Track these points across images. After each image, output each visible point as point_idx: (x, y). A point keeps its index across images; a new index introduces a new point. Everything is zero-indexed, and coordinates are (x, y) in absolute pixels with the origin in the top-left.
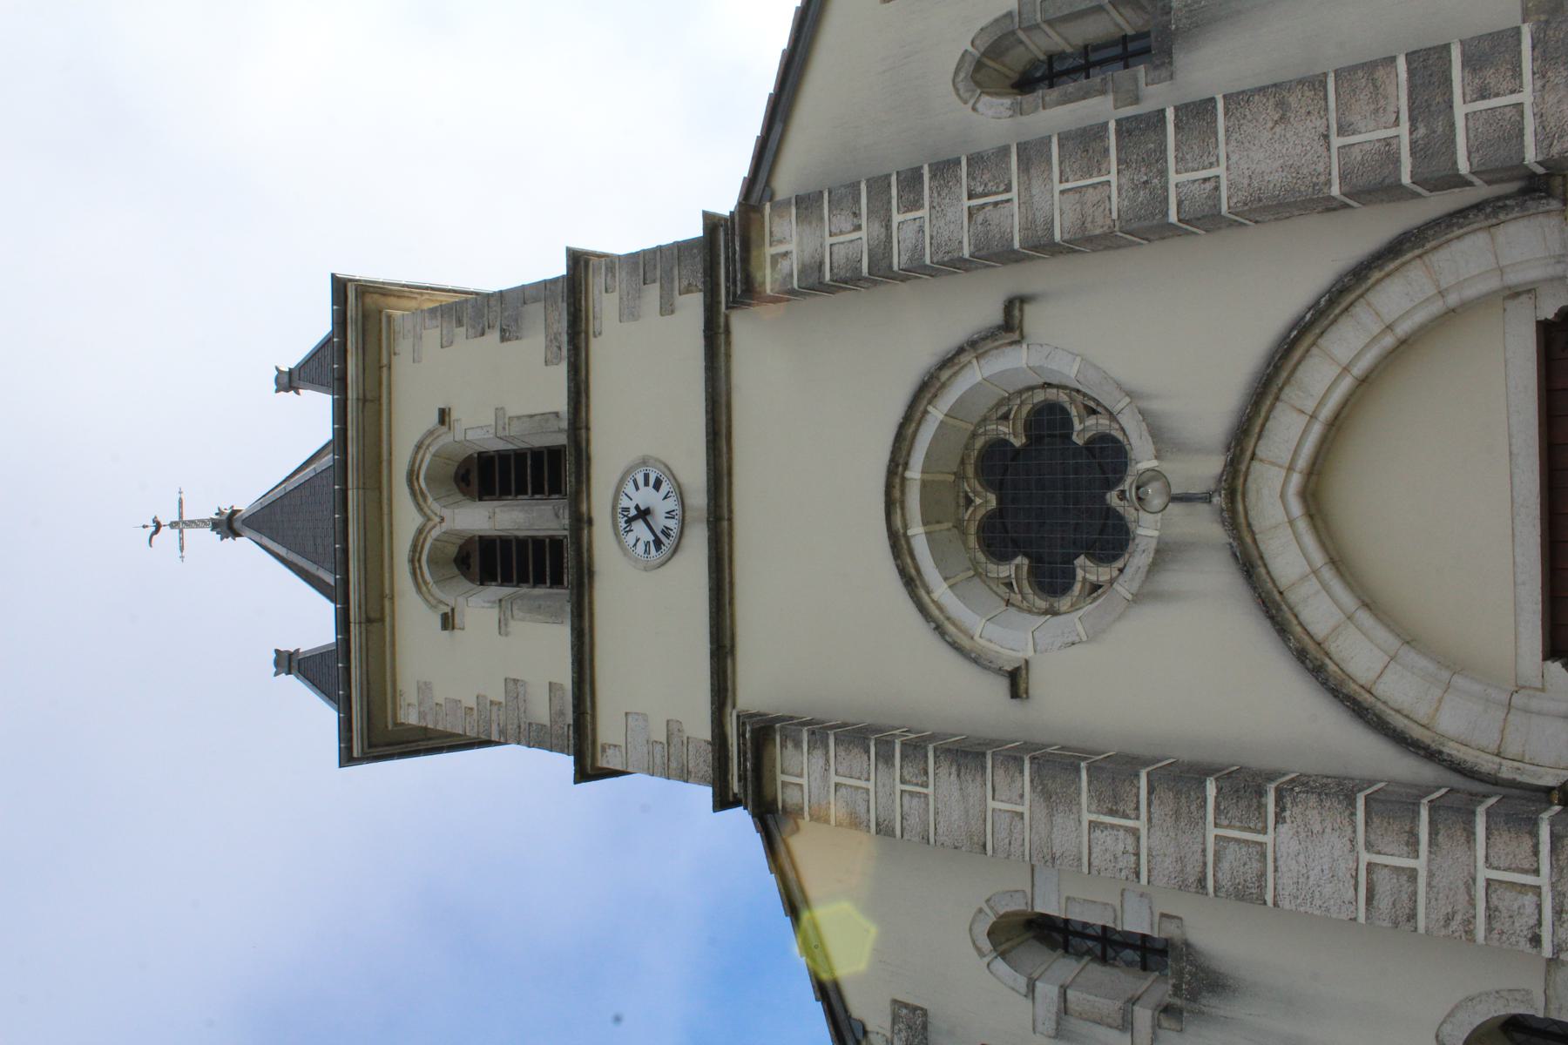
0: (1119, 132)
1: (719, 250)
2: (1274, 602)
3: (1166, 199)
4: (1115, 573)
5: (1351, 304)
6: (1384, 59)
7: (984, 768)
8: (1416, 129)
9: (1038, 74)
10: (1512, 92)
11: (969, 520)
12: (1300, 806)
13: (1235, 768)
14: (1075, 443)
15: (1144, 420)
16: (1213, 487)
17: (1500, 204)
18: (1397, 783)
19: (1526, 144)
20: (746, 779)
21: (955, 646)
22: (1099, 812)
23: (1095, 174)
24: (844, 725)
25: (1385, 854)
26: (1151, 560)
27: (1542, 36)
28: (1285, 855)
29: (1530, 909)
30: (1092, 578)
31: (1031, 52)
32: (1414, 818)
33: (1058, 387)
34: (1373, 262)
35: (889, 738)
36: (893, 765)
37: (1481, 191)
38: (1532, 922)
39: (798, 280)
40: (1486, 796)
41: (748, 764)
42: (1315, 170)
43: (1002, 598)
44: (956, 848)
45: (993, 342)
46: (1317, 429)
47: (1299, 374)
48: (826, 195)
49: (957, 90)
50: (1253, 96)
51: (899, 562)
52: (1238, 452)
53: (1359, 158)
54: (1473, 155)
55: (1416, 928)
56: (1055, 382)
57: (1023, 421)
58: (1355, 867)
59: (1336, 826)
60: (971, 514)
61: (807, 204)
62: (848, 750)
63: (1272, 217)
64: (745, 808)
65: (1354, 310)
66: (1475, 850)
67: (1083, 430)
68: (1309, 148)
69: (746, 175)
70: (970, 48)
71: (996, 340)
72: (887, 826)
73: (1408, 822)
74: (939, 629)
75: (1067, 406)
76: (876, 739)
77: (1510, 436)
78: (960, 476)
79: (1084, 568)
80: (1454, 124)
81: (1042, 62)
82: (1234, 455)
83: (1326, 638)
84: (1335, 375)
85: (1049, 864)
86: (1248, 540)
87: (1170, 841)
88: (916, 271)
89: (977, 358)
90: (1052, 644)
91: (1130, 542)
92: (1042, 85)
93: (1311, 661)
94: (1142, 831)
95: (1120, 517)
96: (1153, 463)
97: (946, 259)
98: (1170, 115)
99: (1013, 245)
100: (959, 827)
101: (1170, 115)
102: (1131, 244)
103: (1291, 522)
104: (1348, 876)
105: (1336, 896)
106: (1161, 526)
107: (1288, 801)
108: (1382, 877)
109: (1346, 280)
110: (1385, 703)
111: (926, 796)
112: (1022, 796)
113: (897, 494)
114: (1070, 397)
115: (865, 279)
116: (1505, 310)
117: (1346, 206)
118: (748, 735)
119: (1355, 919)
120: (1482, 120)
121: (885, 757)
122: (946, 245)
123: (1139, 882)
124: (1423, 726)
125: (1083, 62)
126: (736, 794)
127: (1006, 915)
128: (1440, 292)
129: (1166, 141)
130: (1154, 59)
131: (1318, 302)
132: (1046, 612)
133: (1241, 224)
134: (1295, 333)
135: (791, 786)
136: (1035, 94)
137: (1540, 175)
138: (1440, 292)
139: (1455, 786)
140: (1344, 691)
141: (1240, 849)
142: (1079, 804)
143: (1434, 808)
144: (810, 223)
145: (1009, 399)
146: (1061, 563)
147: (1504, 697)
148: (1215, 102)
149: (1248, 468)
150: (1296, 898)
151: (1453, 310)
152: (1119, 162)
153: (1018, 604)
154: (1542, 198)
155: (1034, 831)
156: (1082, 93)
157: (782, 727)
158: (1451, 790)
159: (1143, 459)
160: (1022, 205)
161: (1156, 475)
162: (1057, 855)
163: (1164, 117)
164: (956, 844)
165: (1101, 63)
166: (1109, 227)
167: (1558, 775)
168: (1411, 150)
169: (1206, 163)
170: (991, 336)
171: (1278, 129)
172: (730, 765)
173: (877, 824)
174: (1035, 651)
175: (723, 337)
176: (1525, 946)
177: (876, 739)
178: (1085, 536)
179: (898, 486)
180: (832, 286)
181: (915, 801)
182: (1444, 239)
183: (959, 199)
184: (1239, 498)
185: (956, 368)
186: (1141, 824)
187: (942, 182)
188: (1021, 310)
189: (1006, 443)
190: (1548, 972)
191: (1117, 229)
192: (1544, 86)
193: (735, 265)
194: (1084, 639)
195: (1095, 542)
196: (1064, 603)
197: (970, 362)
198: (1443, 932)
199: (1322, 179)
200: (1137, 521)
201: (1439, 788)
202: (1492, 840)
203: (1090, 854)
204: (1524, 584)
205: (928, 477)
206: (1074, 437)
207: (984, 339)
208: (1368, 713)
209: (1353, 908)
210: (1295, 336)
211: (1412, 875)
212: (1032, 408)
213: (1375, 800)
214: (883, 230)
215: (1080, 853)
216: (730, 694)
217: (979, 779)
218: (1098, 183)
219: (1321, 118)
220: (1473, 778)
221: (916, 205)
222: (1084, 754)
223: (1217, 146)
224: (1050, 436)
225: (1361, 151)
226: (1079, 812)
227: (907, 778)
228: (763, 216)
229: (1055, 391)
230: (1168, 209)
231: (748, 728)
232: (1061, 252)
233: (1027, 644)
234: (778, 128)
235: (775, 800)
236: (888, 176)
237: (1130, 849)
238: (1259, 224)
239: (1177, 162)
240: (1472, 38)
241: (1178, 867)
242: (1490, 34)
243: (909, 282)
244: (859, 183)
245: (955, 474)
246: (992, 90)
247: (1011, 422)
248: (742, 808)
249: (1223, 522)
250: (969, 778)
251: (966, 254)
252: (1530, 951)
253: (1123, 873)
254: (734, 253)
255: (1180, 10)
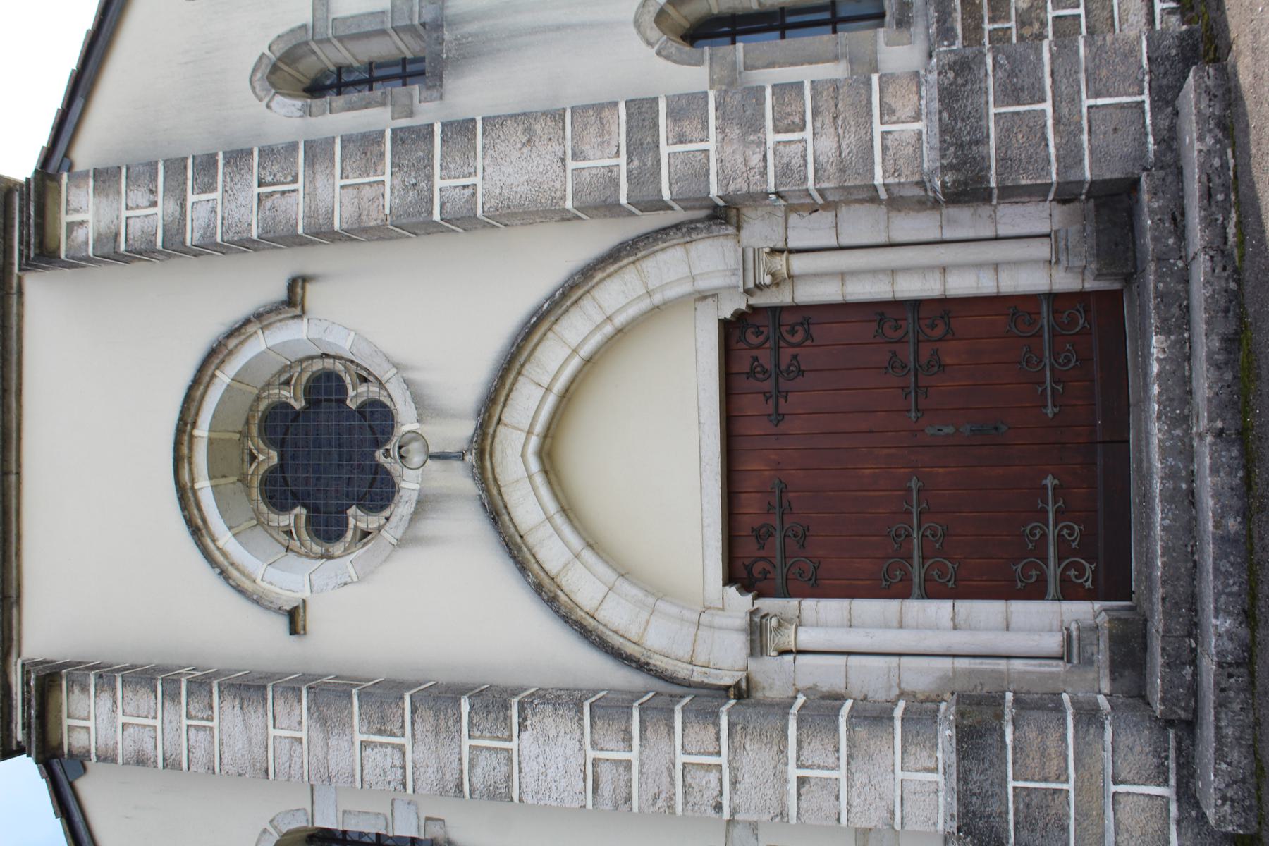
0: (393, 140)
1: (14, 213)
2: (516, 544)
3: (432, 200)
4: (383, 521)
5: (580, 298)
6: (610, 103)
7: (265, 700)
8: (632, 161)
9: (328, 82)
10: (702, 140)
11: (252, 474)
12: (538, 715)
13: (485, 687)
14: (350, 408)
15: (408, 388)
16: (465, 447)
17: (693, 226)
18: (615, 691)
19: (711, 181)
20: (30, 727)
21: (239, 590)
22: (369, 733)
23: (372, 174)
24: (133, 667)
25: (607, 750)
26: (413, 509)
27: (722, 101)
28: (527, 758)
29: (714, 783)
30: (362, 525)
31: (322, 61)
32: (628, 718)
33: (334, 357)
34: (597, 265)
35: (175, 677)
36: (180, 702)
37: (679, 215)
38: (716, 793)
39: (94, 248)
40: (682, 697)
41: (33, 712)
42: (553, 186)
43: (282, 544)
44: (240, 775)
45: (277, 315)
46: (551, 400)
47: (538, 353)
48: (124, 171)
49: (253, 89)
50: (506, 121)
51: (186, 513)
52: (486, 418)
53: (588, 180)
54: (673, 186)
55: (631, 809)
56: (332, 353)
57: (303, 387)
58: (583, 763)
59: (568, 731)
60: (254, 470)
61: (105, 178)
62: (135, 691)
63: (518, 222)
64: (29, 755)
65: (582, 303)
66: (674, 741)
67: (356, 396)
68: (549, 168)
69: (45, 145)
70: (268, 53)
71: (280, 314)
72: (174, 760)
73: (624, 723)
74: (223, 574)
75: (343, 374)
76: (162, 678)
77: (699, 409)
78: (245, 435)
79: (355, 517)
80: (659, 160)
81: (332, 72)
82: (483, 420)
83: (558, 574)
84: (566, 356)
85: (326, 783)
86: (495, 492)
87: (432, 754)
88: (207, 248)
89: (262, 329)
90: (327, 585)
91: (396, 494)
92: (331, 92)
93: (546, 594)
94: (406, 746)
95: (388, 473)
96: (415, 426)
97: (236, 239)
98: (438, 129)
99: (297, 230)
100: (243, 756)
101: (438, 129)
102: (400, 237)
103: (530, 477)
104: (578, 771)
105: (569, 788)
106: (422, 481)
107: (529, 712)
108: (604, 769)
109: (576, 278)
110: (605, 625)
111: (211, 729)
112: (300, 723)
113: (185, 450)
114: (345, 367)
115: (159, 252)
116: (696, 309)
117: (578, 218)
118: (32, 683)
119: (585, 806)
120: (680, 160)
121: (172, 695)
122: (236, 226)
123: (406, 791)
124: (634, 643)
125: (368, 76)
126: (20, 742)
127: (288, 833)
128: (648, 292)
129: (433, 151)
130: (427, 80)
131: (553, 295)
132: (322, 557)
133: (494, 226)
134: (534, 319)
135: (79, 730)
136: (324, 99)
137: (721, 207)
138: (648, 292)
139: (660, 690)
140: (573, 617)
141: (490, 755)
142: (352, 727)
143: (643, 709)
144: (107, 196)
145: (291, 367)
146: (335, 513)
147: (695, 617)
148: (476, 123)
149: (495, 431)
150: (537, 793)
151: (658, 307)
152: (393, 164)
153: (298, 550)
154: (722, 224)
155: (311, 754)
156: (364, 103)
157: (69, 673)
158: (657, 694)
159: (407, 422)
160: (306, 195)
161: (416, 436)
162: (333, 774)
163: (433, 131)
164: (240, 771)
165: (383, 79)
166: (382, 221)
167: (733, 676)
168: (627, 176)
169: (466, 173)
170: (276, 310)
171: (525, 150)
172: (14, 713)
173: (164, 759)
174: (312, 592)
175: (14, 298)
176: (711, 813)
177: (162, 678)
178: (356, 489)
179: (186, 443)
180: (126, 256)
181: (201, 734)
182: (651, 250)
183: (250, 186)
184: (487, 457)
185: (243, 337)
186: (406, 741)
187: (235, 169)
188: (303, 288)
189: (286, 405)
190: (728, 831)
191: (388, 222)
192: (723, 139)
193: (29, 229)
194: (355, 579)
195: (366, 494)
196: (338, 548)
197: (256, 332)
198: (652, 809)
199: (559, 194)
200: (401, 476)
201: (647, 693)
202: (687, 731)
203: (362, 771)
204: (709, 525)
205: (215, 435)
206: (348, 402)
207: (269, 312)
208: (592, 635)
209: (582, 797)
210: (535, 322)
211: (628, 765)
212: (311, 376)
213: (599, 706)
214: (178, 208)
215: (354, 770)
216: (15, 643)
217: (261, 710)
218: (375, 182)
219: (560, 144)
220: (673, 683)
221: (210, 187)
222: (356, 681)
223: (475, 159)
224: (326, 400)
225: (590, 174)
226: (352, 734)
227: (193, 713)
228: (60, 186)
229: (332, 361)
230: (432, 209)
231: (33, 676)
232: (340, 240)
233: (304, 586)
234: (78, 103)
235: (61, 744)
236: (185, 159)
237: (397, 763)
238: (508, 228)
239: (442, 170)
240: (674, 96)
241: (439, 776)
242: (687, 94)
243: (201, 257)
244: (156, 163)
245: (240, 432)
246: (286, 92)
247: (292, 387)
248: (25, 755)
249: (474, 478)
250: (251, 709)
251: (255, 236)
252: (714, 816)
253: (391, 785)
254: (29, 218)
255: (451, 42)
